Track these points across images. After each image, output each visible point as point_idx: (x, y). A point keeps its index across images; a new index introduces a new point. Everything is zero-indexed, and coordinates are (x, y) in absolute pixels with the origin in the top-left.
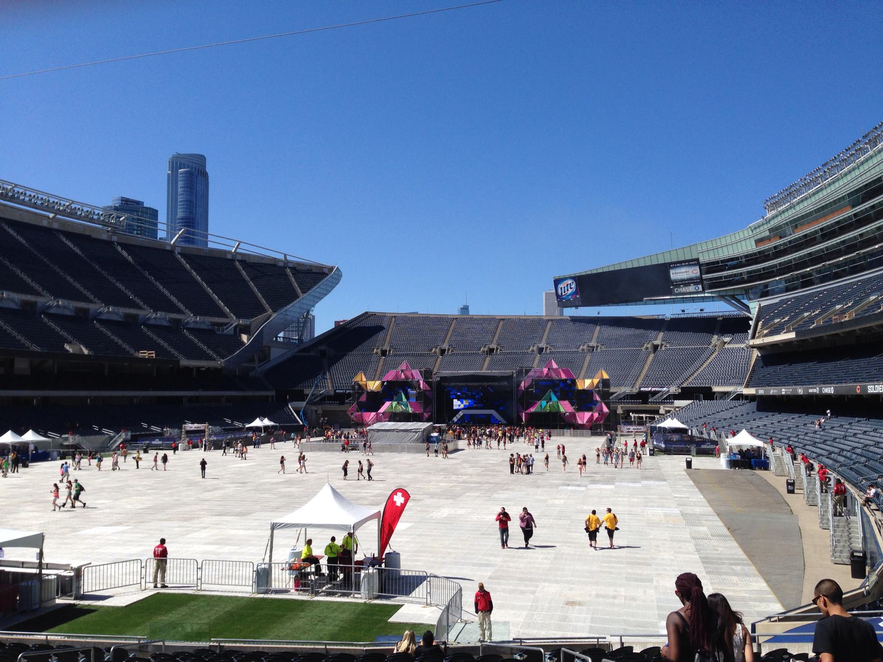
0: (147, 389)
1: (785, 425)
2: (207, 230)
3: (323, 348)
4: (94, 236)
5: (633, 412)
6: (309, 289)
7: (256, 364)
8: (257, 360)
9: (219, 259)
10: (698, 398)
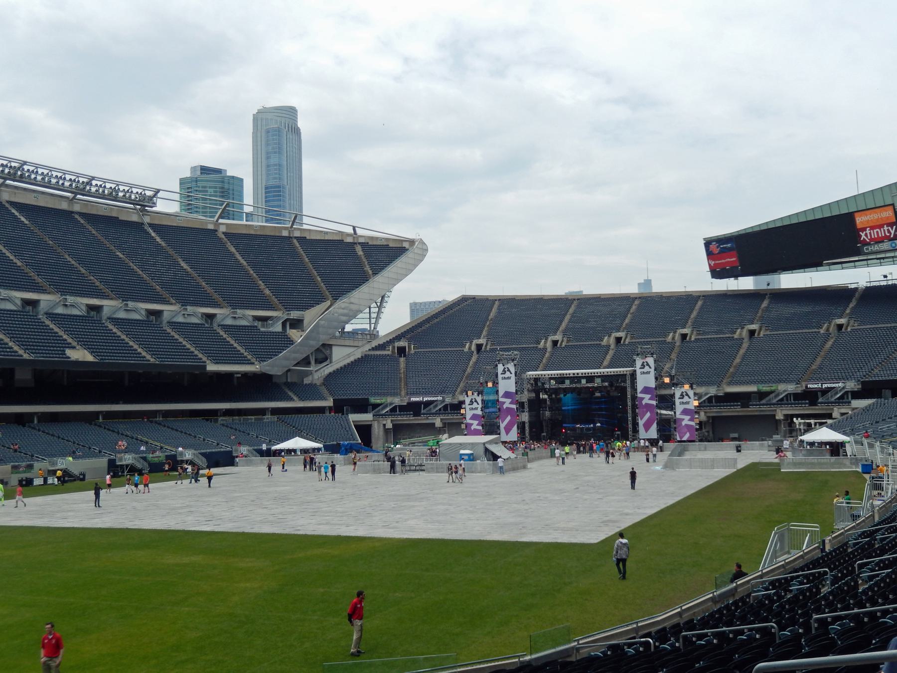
0: (117, 402)
1: (131, 523)
2: (242, 200)
3: (402, 343)
4: (123, 217)
5: (797, 416)
6: (382, 269)
7: (312, 368)
8: (313, 362)
9: (109, 223)
10: (879, 396)
